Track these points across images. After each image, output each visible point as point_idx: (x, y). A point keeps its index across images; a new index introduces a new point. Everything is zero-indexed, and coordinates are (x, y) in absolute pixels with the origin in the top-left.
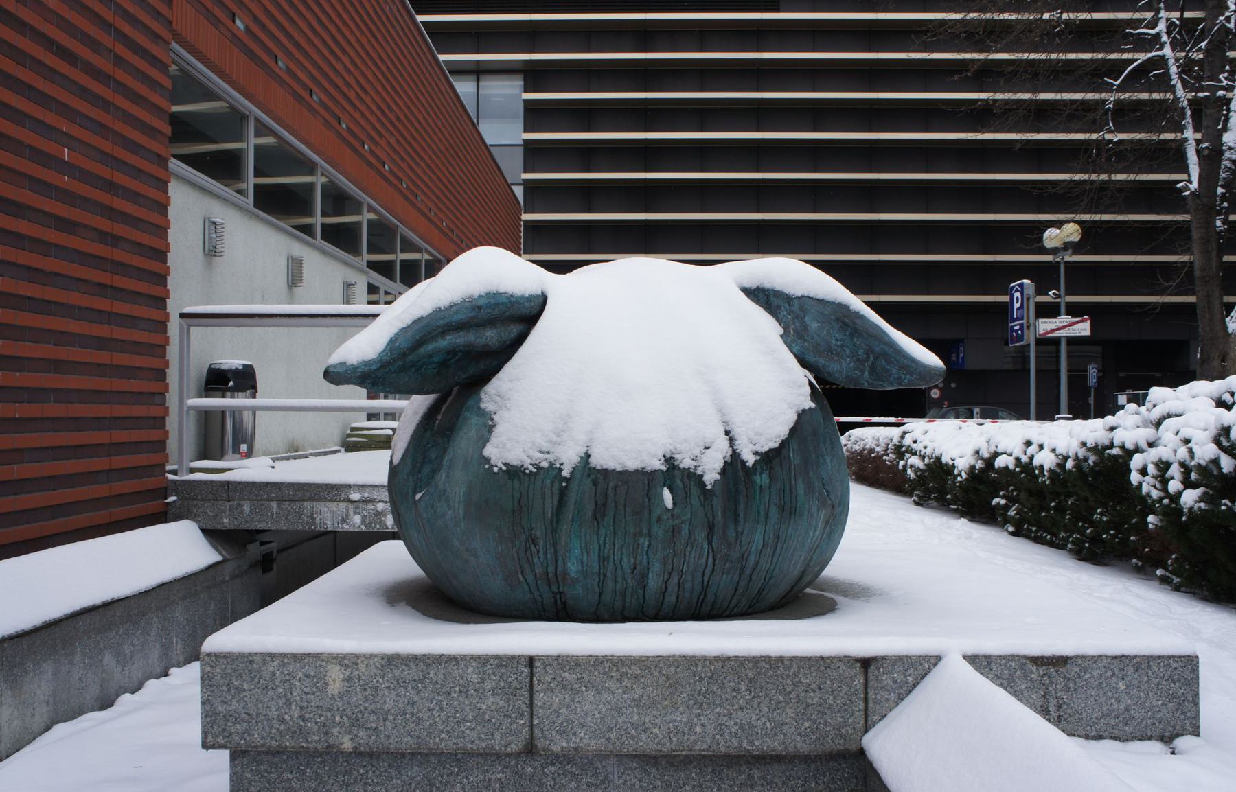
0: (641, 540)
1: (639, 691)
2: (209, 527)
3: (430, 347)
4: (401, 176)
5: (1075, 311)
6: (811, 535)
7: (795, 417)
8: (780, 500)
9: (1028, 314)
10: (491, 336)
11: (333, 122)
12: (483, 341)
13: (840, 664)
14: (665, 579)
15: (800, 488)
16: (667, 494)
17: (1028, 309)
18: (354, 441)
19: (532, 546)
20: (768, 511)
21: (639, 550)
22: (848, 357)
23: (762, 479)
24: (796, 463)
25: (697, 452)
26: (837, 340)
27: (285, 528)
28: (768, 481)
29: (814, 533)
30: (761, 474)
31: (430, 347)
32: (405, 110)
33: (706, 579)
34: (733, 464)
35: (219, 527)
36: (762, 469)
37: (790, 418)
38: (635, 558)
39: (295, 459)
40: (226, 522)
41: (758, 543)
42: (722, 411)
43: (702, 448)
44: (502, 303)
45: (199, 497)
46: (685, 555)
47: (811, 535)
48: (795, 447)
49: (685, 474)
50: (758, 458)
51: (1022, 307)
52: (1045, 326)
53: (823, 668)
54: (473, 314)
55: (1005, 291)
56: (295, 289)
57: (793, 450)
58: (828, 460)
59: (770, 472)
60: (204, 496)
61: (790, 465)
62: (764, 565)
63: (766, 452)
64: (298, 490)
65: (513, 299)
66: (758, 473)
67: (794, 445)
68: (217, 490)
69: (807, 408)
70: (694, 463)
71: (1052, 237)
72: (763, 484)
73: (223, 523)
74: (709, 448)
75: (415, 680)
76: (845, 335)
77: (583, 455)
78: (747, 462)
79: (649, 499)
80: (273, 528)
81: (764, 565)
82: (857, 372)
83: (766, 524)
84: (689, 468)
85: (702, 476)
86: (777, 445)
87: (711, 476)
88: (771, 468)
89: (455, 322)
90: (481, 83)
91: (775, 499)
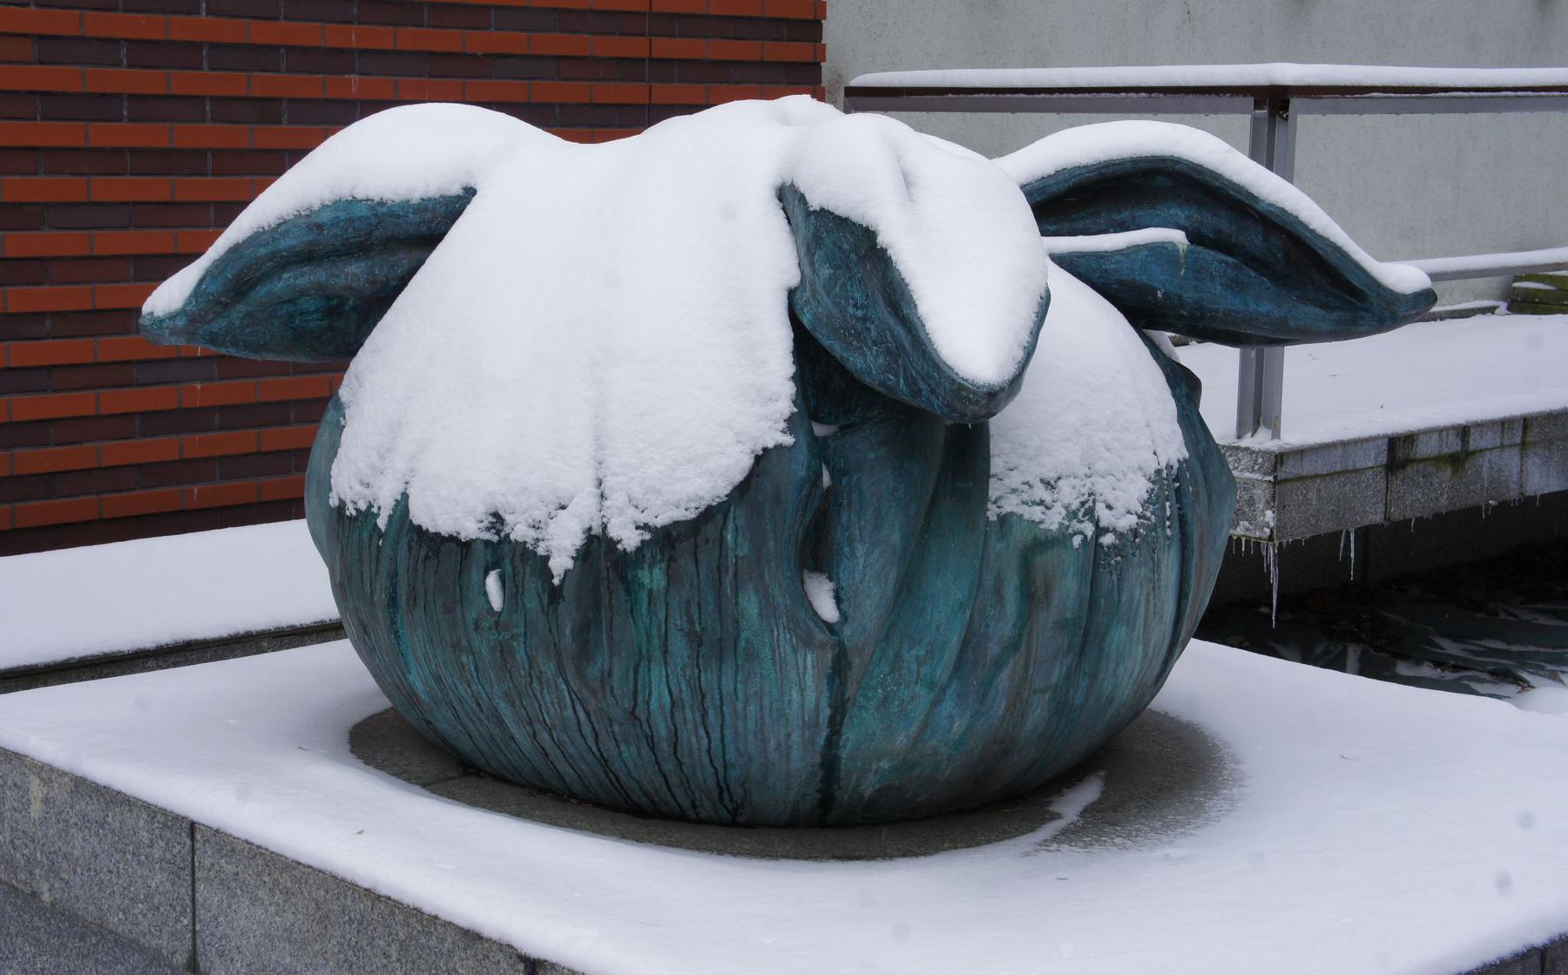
1: (291, 917)
6: (795, 695)
7: (748, 462)
8: (691, 621)
10: (354, 273)
12: (341, 281)
13: (500, 956)
14: (531, 733)
16: (492, 583)
18: (1527, 290)
20: (666, 640)
22: (875, 343)
23: (653, 577)
24: (740, 553)
25: (540, 514)
26: (855, 306)
28: (663, 583)
29: (802, 691)
30: (651, 567)
34: (596, 546)
36: (653, 557)
37: (737, 464)
39: (1442, 319)
41: (660, 696)
42: (599, 442)
43: (552, 507)
44: (360, 218)
46: (535, 695)
47: (795, 695)
48: (741, 522)
49: (519, 552)
50: (647, 536)
53: (480, 956)
54: (310, 237)
57: (736, 529)
58: (861, 550)
59: (668, 567)
61: (722, 555)
62: (694, 740)
63: (664, 528)
65: (381, 210)
66: (646, 566)
67: (738, 516)
69: (771, 445)
70: (532, 534)
72: (655, 588)
74: (563, 507)
75: (97, 822)
77: (399, 498)
78: (619, 542)
79: (461, 588)
81: (694, 740)
83: (666, 664)
84: (525, 543)
85: (547, 558)
86: (691, 515)
87: (560, 563)
88: (672, 560)
89: (286, 251)
91: (678, 620)
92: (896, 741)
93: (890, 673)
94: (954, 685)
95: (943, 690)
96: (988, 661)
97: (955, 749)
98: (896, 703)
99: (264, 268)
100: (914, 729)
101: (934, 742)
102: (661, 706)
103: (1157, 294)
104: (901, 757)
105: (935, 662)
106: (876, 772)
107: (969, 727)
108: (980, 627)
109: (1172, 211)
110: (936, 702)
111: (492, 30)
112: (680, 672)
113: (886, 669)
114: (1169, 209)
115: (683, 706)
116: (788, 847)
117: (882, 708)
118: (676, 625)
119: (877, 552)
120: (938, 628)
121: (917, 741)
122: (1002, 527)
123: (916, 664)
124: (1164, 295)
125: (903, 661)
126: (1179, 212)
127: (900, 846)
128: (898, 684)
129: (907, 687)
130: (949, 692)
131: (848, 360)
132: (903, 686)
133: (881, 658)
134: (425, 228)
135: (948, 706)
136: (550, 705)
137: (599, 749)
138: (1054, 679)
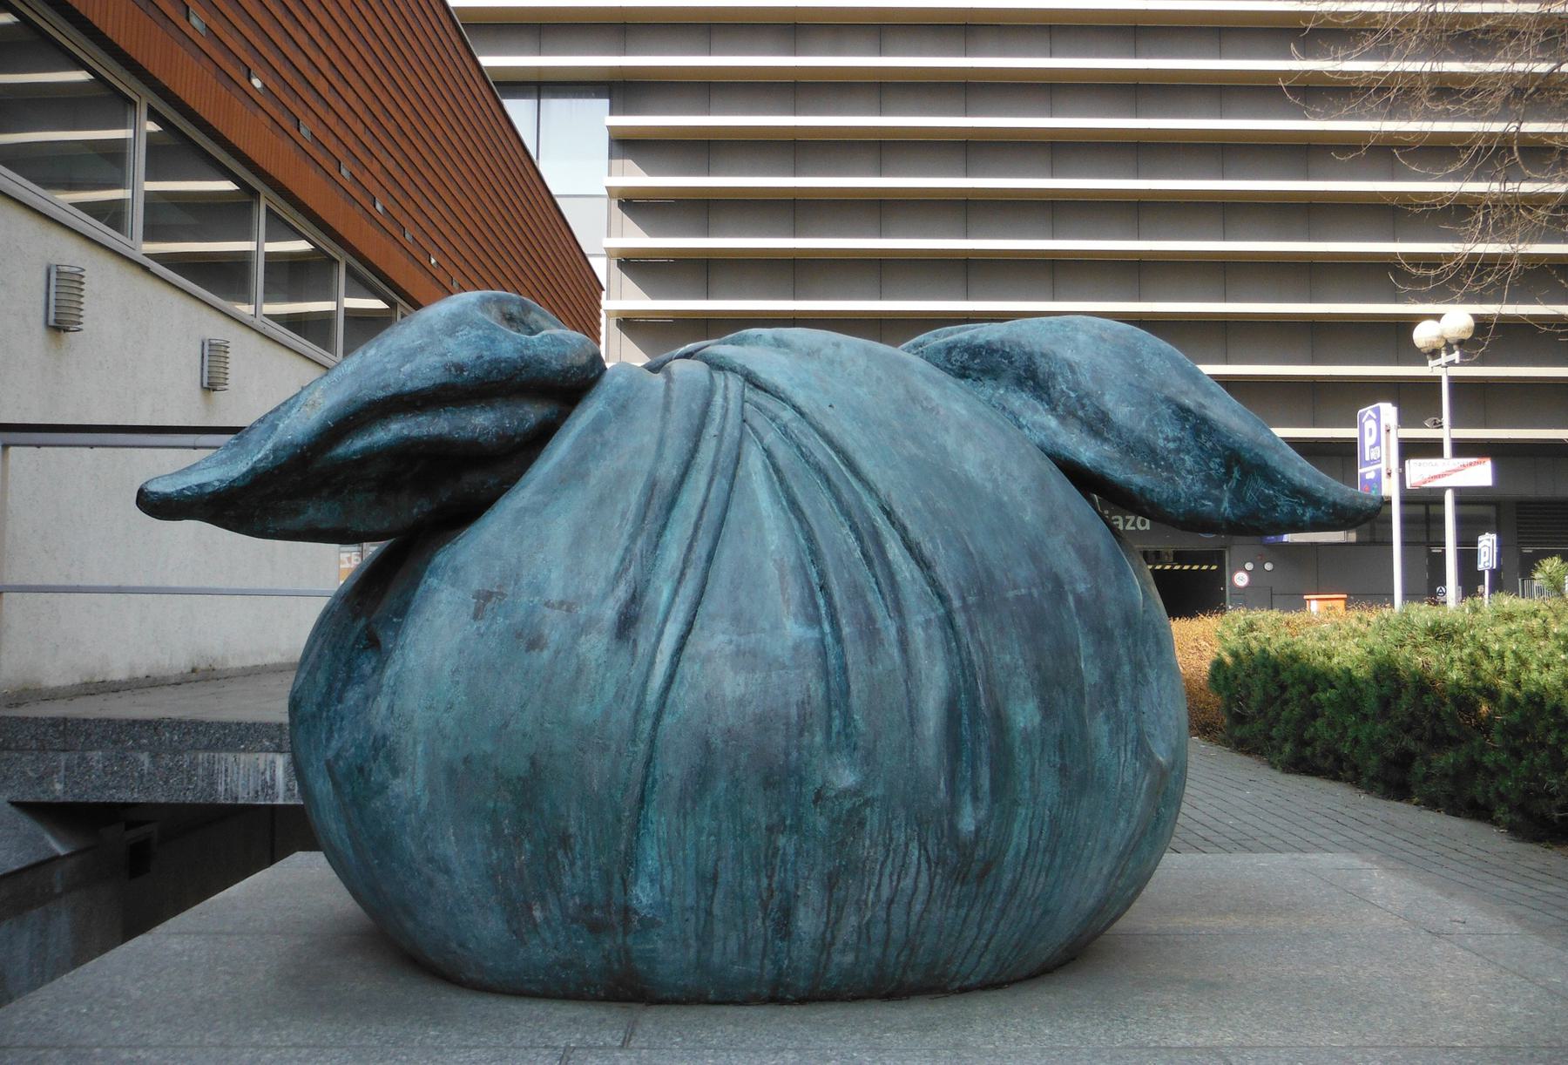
0: (782, 841)
2: (29, 798)
3: (358, 444)
4: (339, 153)
5: (1463, 449)
9: (1388, 455)
11: (288, 124)
15: (1100, 728)
17: (1388, 447)
19: (560, 853)
21: (778, 860)
22: (1190, 472)
26: (1167, 439)
27: (163, 800)
31: (358, 444)
32: (413, 118)
33: (914, 918)
35: (45, 798)
38: (770, 878)
40: (58, 790)
45: (13, 745)
51: (1378, 443)
52: (1421, 472)
55: (1352, 423)
56: (217, 396)
60: (21, 743)
62: (1030, 889)
64: (189, 733)
68: (45, 734)
71: (1423, 335)
73: (53, 792)
76: (1183, 429)
80: (143, 799)
82: (1207, 503)
90: (542, 101)
102: (1018, 853)
118: (1049, 761)
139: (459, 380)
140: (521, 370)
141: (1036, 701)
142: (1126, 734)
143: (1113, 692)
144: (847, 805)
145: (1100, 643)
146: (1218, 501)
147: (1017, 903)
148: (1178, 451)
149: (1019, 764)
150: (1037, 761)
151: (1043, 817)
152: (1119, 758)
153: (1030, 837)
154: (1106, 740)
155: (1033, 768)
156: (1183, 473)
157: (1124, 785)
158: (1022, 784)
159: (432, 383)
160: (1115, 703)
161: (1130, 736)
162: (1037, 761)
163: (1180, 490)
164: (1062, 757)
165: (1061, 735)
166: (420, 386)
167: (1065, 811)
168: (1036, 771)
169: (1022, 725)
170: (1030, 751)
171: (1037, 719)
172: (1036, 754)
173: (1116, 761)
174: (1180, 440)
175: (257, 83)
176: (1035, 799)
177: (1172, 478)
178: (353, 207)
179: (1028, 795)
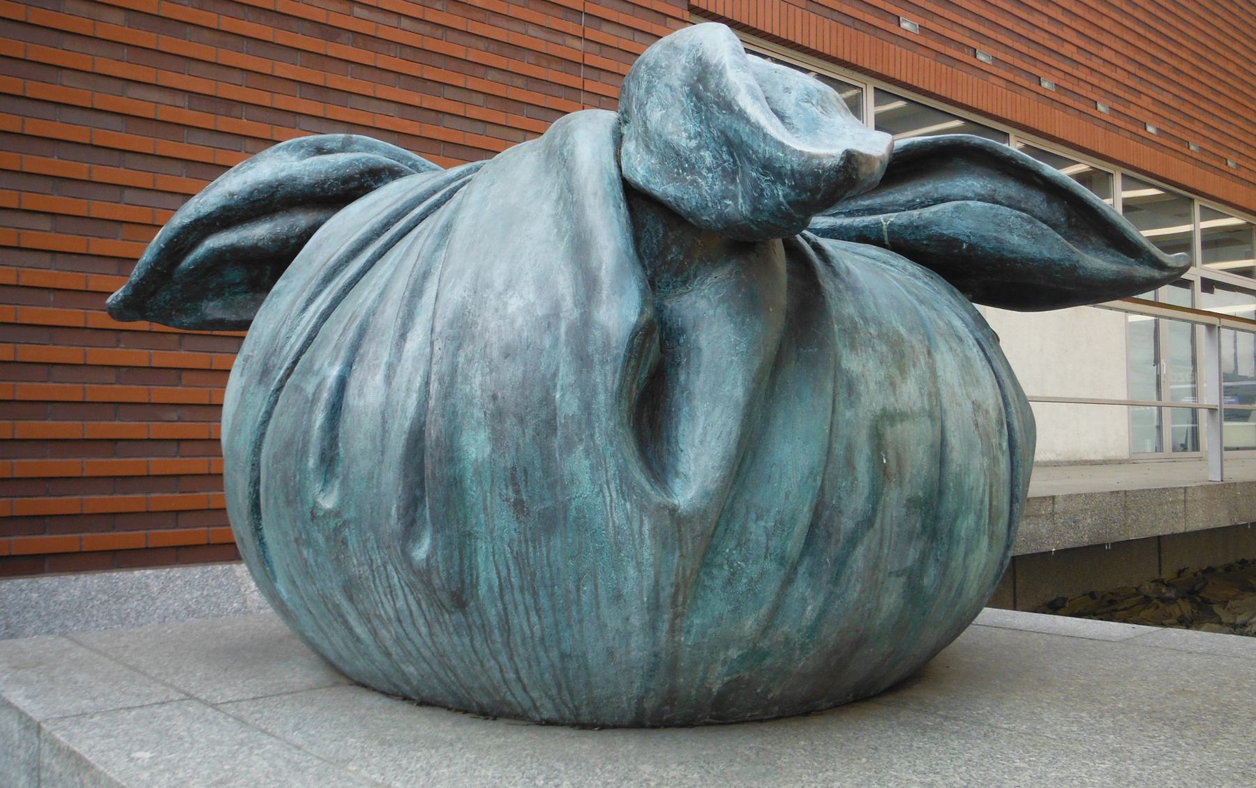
62: (526, 628)
92: (745, 625)
93: (737, 546)
94: (806, 563)
95: (794, 568)
96: (841, 538)
97: (808, 637)
98: (744, 581)
99: (191, 238)
100: (764, 611)
101: (786, 628)
102: (490, 588)
103: (962, 246)
104: (751, 645)
105: (786, 534)
106: (724, 662)
107: (822, 613)
108: (832, 499)
109: (970, 182)
110: (788, 582)
111: (397, 59)
112: (507, 548)
113: (732, 544)
114: (966, 181)
115: (512, 589)
116: (631, 747)
117: (729, 588)
118: (500, 495)
119: (718, 411)
120: (787, 496)
121: (766, 628)
122: (849, 396)
123: (764, 537)
124: (967, 247)
125: (751, 533)
126: (975, 183)
127: (752, 745)
128: (746, 560)
129: (756, 562)
130: (802, 570)
131: (683, 199)
132: (751, 562)
133: (726, 530)
134: (318, 190)
135: (801, 587)
136: (383, 597)
137: (434, 642)
138: (909, 564)
139: (233, 202)
140: (277, 188)
141: (488, 431)
142: (607, 472)
143: (590, 424)
144: (332, 524)
145: (581, 372)
146: (734, 198)
147: (519, 640)
148: (699, 148)
149: (472, 496)
150: (488, 494)
151: (504, 553)
152: (604, 497)
153: (498, 573)
154: (587, 476)
155: (485, 500)
156: (704, 172)
157: (618, 531)
158: (477, 517)
159: (215, 207)
160: (592, 435)
161: (611, 473)
162: (488, 494)
163: (704, 193)
164: (517, 492)
165: (514, 469)
166: (209, 211)
167: (531, 549)
168: (489, 504)
169: (474, 456)
170: (480, 483)
171: (488, 450)
172: (487, 487)
173: (600, 499)
174: (700, 134)
175: (905, 25)
176: (491, 533)
177: (695, 181)
178: (1140, 98)
179: (483, 528)
